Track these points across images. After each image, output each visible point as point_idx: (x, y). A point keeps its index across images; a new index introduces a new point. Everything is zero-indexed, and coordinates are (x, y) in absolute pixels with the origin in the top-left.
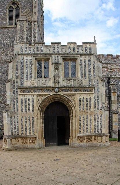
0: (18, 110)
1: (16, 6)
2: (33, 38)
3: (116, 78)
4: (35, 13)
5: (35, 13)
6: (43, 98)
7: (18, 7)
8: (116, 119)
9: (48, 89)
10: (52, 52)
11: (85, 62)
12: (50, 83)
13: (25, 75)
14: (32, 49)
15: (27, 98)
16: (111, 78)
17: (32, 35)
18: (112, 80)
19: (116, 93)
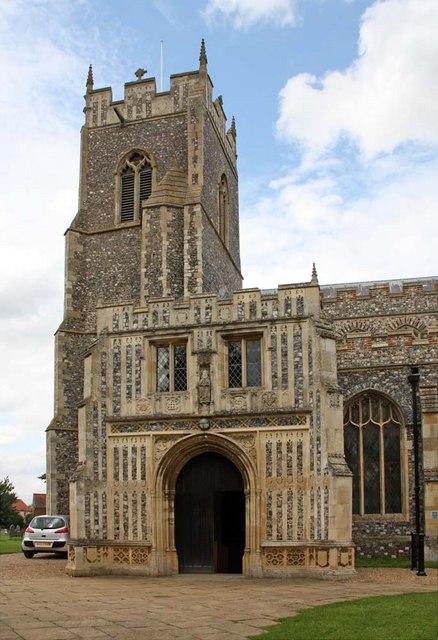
1: (142, 162)
2: (187, 257)
5: (196, 177)
6: (170, 445)
9: (182, 420)
10: (192, 321)
11: (284, 341)
12: (187, 405)
13: (123, 386)
14: (141, 317)
15: (130, 445)
16: (423, 365)
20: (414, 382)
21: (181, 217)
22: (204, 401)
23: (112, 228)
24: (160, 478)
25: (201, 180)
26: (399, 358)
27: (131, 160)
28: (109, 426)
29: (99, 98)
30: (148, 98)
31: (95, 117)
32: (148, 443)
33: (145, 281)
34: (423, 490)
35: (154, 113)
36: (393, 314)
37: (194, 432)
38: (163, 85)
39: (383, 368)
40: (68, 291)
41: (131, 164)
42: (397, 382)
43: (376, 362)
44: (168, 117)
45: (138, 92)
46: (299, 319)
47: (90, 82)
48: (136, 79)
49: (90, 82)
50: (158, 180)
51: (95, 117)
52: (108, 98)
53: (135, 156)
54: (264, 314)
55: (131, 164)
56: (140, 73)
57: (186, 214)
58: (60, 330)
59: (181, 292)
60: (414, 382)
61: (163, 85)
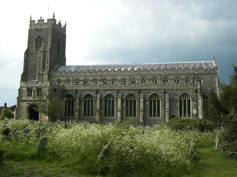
0: (20, 109)
1: (40, 38)
2: (46, 62)
3: (81, 90)
4: (49, 44)
5: (49, 44)
6: (29, 104)
7: (41, 39)
8: (77, 114)
9: (31, 101)
10: (33, 86)
11: (45, 90)
12: (31, 99)
13: (23, 95)
14: (26, 85)
15: (23, 104)
16: (78, 90)
17: (46, 60)
18: (78, 91)
19: (78, 99)
20: (76, 93)
21: (46, 54)
22: (34, 98)
23: (33, 53)
24: (27, 110)
25: (50, 45)
26: (74, 88)
27: (38, 38)
28: (21, 101)
29: (32, 23)
30: (42, 24)
31: (31, 27)
32: (26, 104)
33: (38, 67)
34: (202, 117)
35: (43, 27)
36: (84, 76)
37: (32, 103)
38: (46, 21)
39: (71, 90)
40: (24, 67)
41: (38, 39)
42: (74, 93)
43: (70, 89)
44: (46, 29)
45: (41, 22)
46: (47, 87)
47: (31, 18)
48: (40, 19)
49: (31, 18)
50: (43, 43)
51: (31, 27)
52: (34, 23)
53: (39, 37)
55: (38, 39)
56: (41, 18)
57: (47, 53)
58: (22, 74)
59: (45, 69)
60: (76, 93)
61: (46, 21)
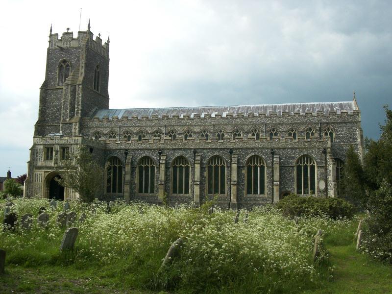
0: (33, 180)
1: (66, 64)
2: (76, 103)
3: (134, 149)
4: (82, 73)
5: (82, 73)
6: (48, 173)
7: (68, 66)
8: (127, 189)
9: (51, 168)
10: (54, 143)
11: (74, 149)
12: (52, 164)
13: (38, 158)
14: (43, 141)
15: (39, 173)
16: (129, 149)
17: (76, 99)
18: (129, 152)
19: (130, 165)
20: (126, 154)
21: (75, 89)
22: (56, 162)
23: (54, 88)
24: (45, 182)
25: (83, 75)
26: (123, 147)
27: (63, 63)
29: (54, 37)
30: (70, 40)
31: (52, 45)
32: (43, 173)
33: (63, 111)
34: (334, 194)
35: (72, 45)
36: (138, 126)
37: (53, 171)
38: (75, 36)
39: (118, 150)
40: (40, 110)
41: (63, 64)
42: (122, 154)
43: (116, 147)
45: (67, 37)
47: (51, 31)
48: (66, 31)
49: (51, 31)
51: (52, 45)
52: (57, 38)
53: (64, 61)
54: (70, 142)
55: (63, 64)
56: (68, 29)
57: (77, 88)
58: (36, 124)
59: (74, 115)
60: (126, 154)
61: (75, 36)
